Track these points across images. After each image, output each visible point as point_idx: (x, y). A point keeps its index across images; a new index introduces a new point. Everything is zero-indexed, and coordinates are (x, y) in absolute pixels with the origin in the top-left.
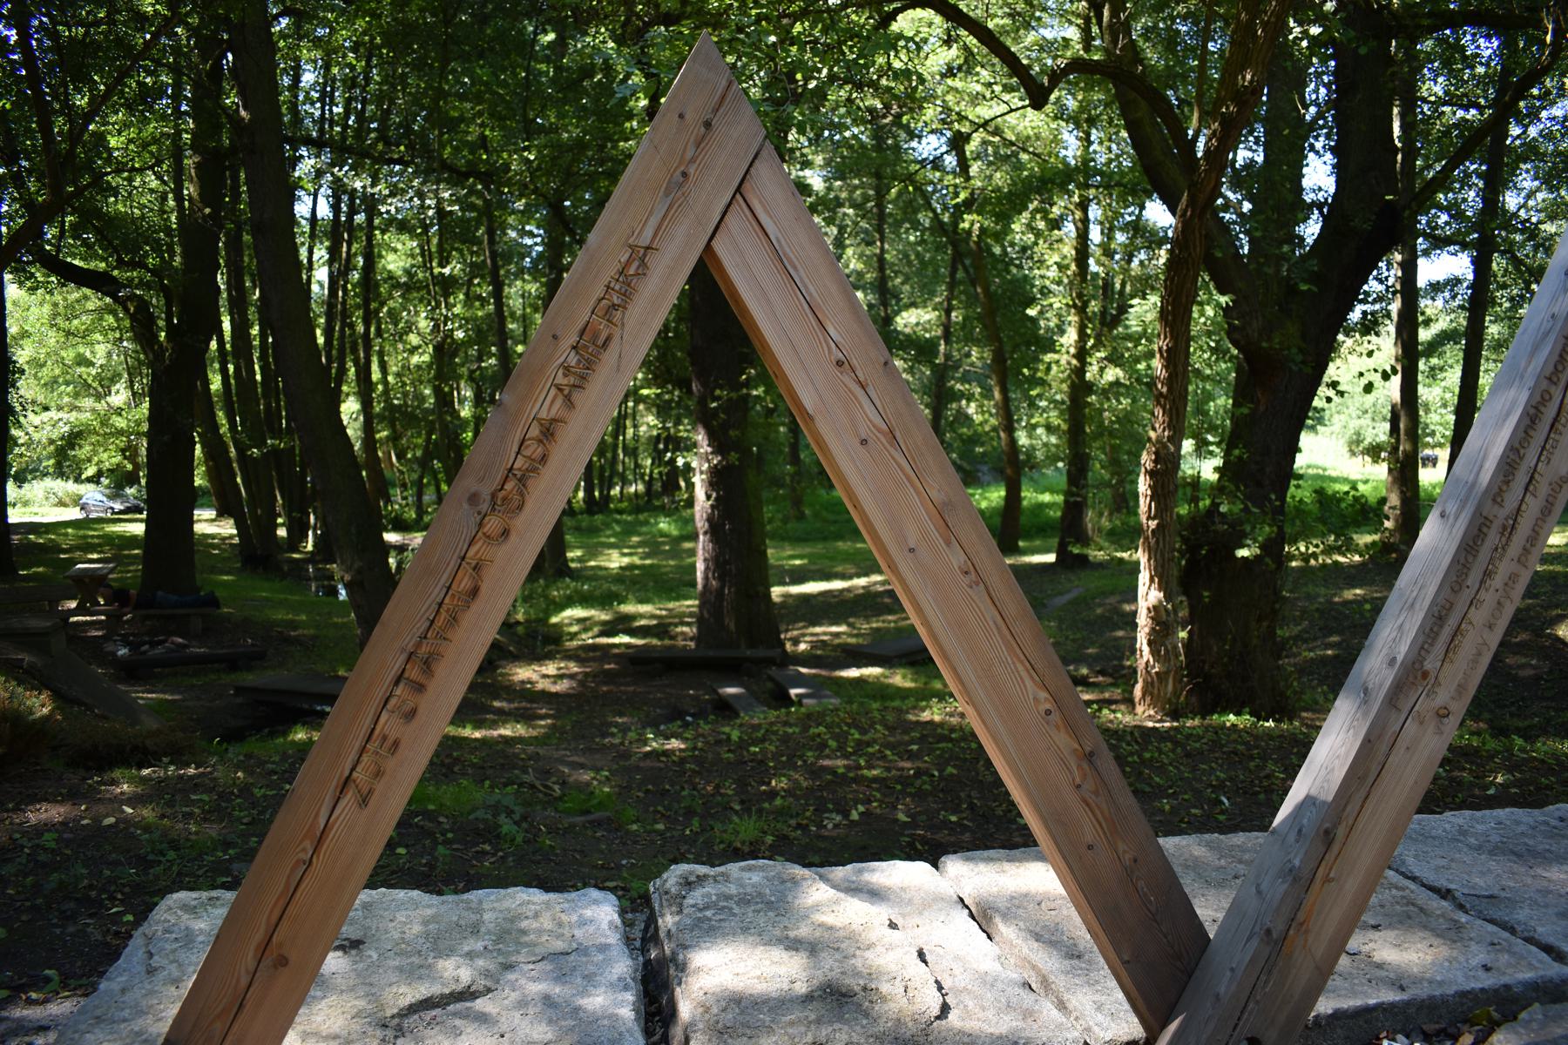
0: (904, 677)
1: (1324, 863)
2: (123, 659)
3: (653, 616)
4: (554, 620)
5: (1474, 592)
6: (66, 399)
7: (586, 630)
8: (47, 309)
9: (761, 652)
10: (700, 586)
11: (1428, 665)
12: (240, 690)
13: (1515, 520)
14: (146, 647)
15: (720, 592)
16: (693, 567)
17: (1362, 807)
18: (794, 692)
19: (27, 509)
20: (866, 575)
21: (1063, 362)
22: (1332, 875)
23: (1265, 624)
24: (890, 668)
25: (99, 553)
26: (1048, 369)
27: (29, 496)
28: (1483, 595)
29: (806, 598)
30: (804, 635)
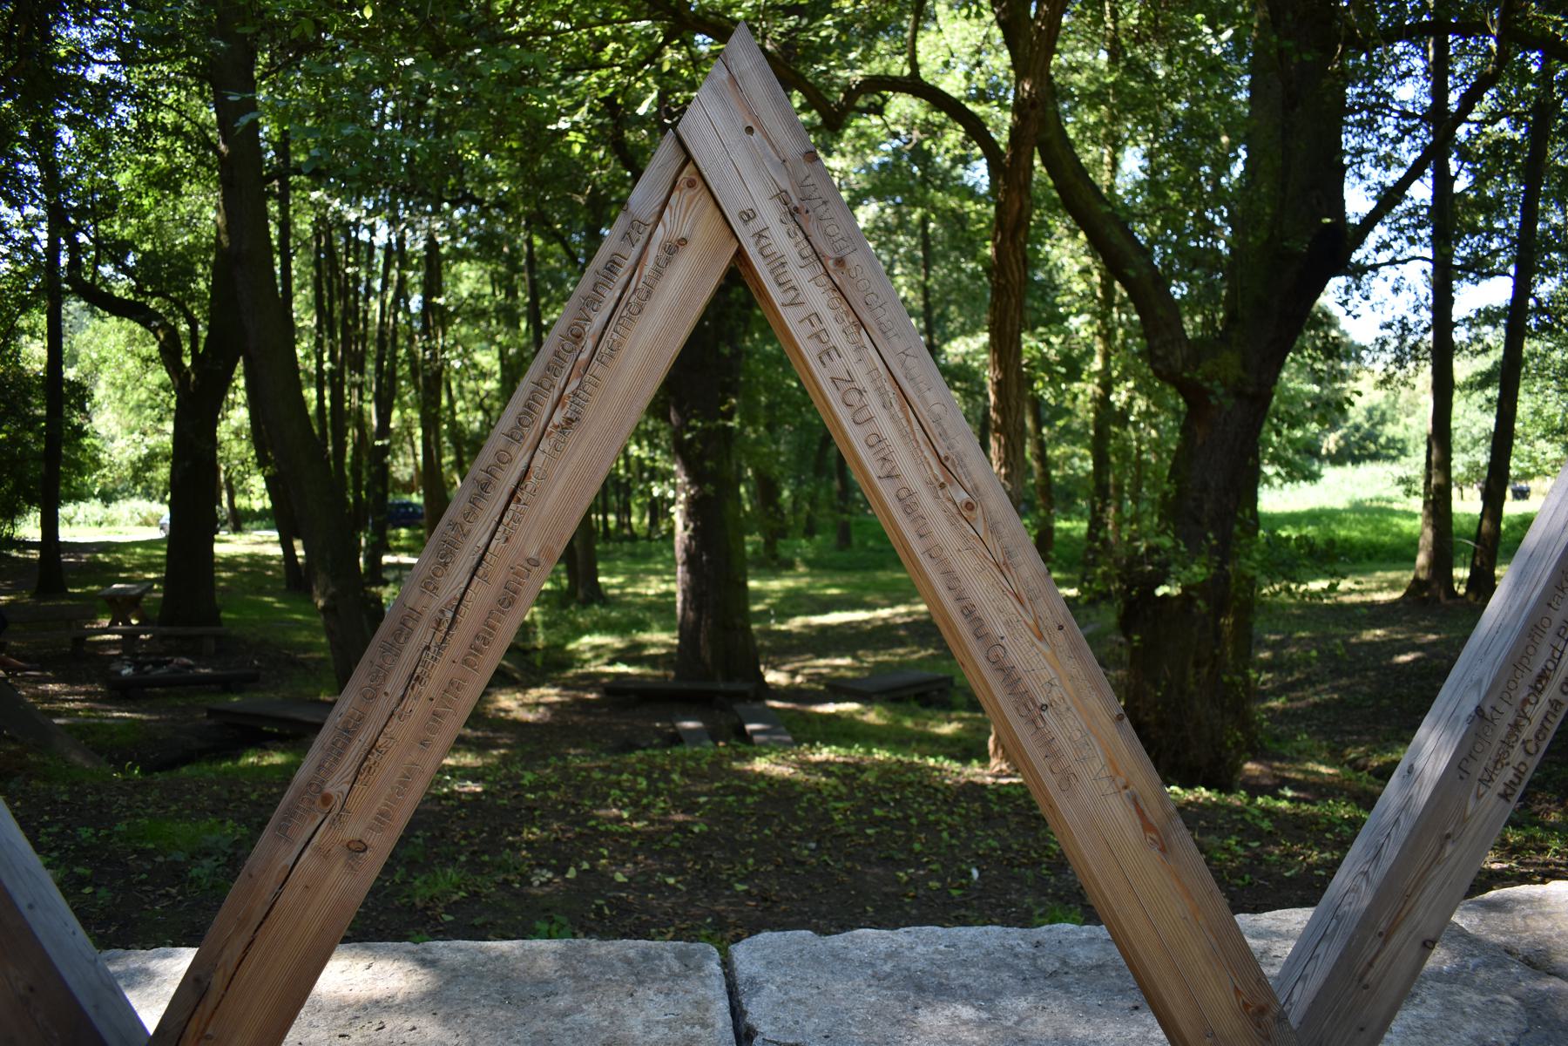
0: (879, 715)
1: (196, 1016)
2: (127, 679)
3: (665, 645)
4: (571, 646)
5: (395, 700)
6: (149, 423)
7: (597, 657)
8: (123, 336)
9: (738, 686)
10: (679, 618)
11: (330, 788)
12: (212, 713)
13: (456, 612)
14: (149, 667)
15: (697, 623)
16: (675, 603)
17: (245, 953)
18: (750, 727)
19: (112, 528)
20: (892, 606)
21: (1089, 392)
22: (209, 1031)
23: (1205, 671)
24: (867, 705)
25: (156, 572)
26: (1075, 397)
27: (115, 515)
28: (410, 703)
29: (824, 629)
30: (804, 667)
